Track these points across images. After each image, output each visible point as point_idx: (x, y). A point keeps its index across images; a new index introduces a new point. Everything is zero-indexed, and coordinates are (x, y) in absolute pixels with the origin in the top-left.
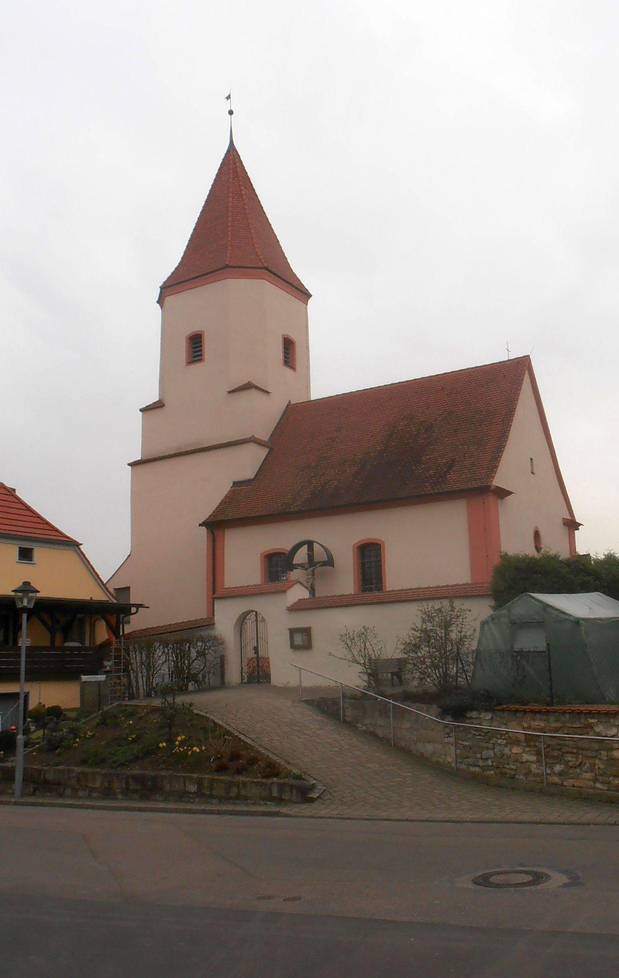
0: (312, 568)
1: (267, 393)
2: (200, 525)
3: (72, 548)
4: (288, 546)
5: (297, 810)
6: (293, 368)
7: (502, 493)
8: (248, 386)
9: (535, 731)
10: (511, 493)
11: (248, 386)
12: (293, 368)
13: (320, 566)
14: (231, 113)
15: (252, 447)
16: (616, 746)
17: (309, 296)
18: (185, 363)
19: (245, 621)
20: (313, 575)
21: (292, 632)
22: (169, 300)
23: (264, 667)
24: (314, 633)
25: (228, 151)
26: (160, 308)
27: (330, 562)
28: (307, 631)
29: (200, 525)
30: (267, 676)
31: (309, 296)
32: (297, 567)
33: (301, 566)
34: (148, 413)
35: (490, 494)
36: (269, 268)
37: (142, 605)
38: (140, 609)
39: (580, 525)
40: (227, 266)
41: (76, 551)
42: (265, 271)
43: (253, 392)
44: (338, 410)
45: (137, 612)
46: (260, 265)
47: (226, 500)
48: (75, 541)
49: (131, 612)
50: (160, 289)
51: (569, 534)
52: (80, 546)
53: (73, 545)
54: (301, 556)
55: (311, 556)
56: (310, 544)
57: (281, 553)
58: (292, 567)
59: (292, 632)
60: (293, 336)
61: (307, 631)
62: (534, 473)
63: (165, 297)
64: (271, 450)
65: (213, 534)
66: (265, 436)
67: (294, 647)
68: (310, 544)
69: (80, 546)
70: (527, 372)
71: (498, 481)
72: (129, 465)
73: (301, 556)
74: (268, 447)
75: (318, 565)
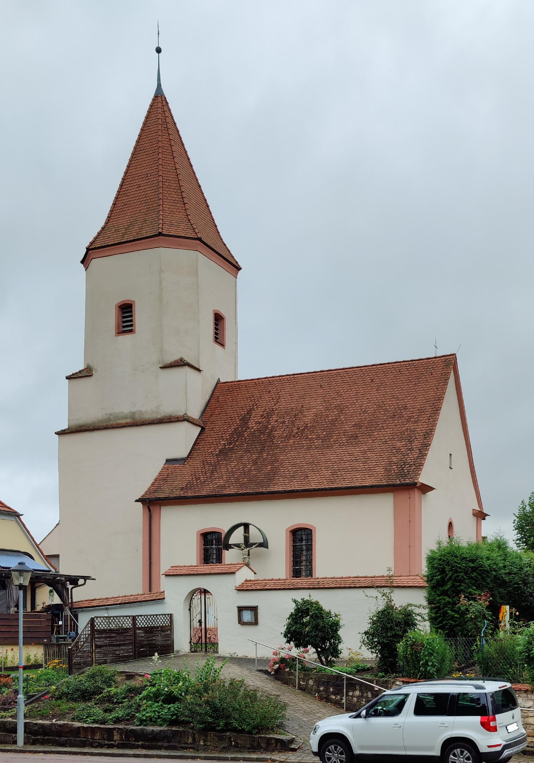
0: (248, 549)
1: (199, 370)
2: (137, 501)
3: (13, 519)
4: (225, 528)
5: (285, 757)
6: (222, 345)
7: (425, 489)
8: (181, 363)
9: (467, 702)
10: (434, 489)
11: (181, 363)
12: (222, 345)
13: (256, 547)
14: (159, 50)
15: (186, 425)
16: (531, 714)
17: (239, 269)
18: (113, 332)
19: (193, 597)
20: (249, 555)
21: (241, 609)
22: (95, 263)
23: (212, 639)
24: (260, 611)
25: (156, 96)
26: (84, 270)
27: (264, 545)
28: (254, 609)
29: (137, 501)
30: (215, 645)
31: (239, 269)
32: (234, 547)
33: (238, 546)
34: (74, 382)
35: (416, 490)
36: (203, 239)
37: (90, 577)
38: (87, 581)
39: (487, 515)
40: (160, 234)
41: (17, 521)
42: (199, 242)
43: (187, 369)
44: (269, 393)
45: (84, 584)
46: (193, 235)
47: (161, 477)
48: (16, 512)
49: (78, 583)
50: (86, 250)
51: (477, 525)
52: (21, 517)
53: (15, 515)
54: (237, 537)
55: (246, 539)
56: (246, 526)
57: (217, 532)
58: (228, 547)
59: (241, 609)
60: (223, 312)
61: (254, 609)
62: (451, 468)
63: (92, 259)
64: (203, 429)
65: (150, 511)
66: (195, 413)
67: (241, 622)
68: (246, 526)
69: (21, 517)
70: (452, 373)
71: (423, 479)
72: (67, 378)
73: (237, 537)
74: (199, 426)
75: (254, 546)
